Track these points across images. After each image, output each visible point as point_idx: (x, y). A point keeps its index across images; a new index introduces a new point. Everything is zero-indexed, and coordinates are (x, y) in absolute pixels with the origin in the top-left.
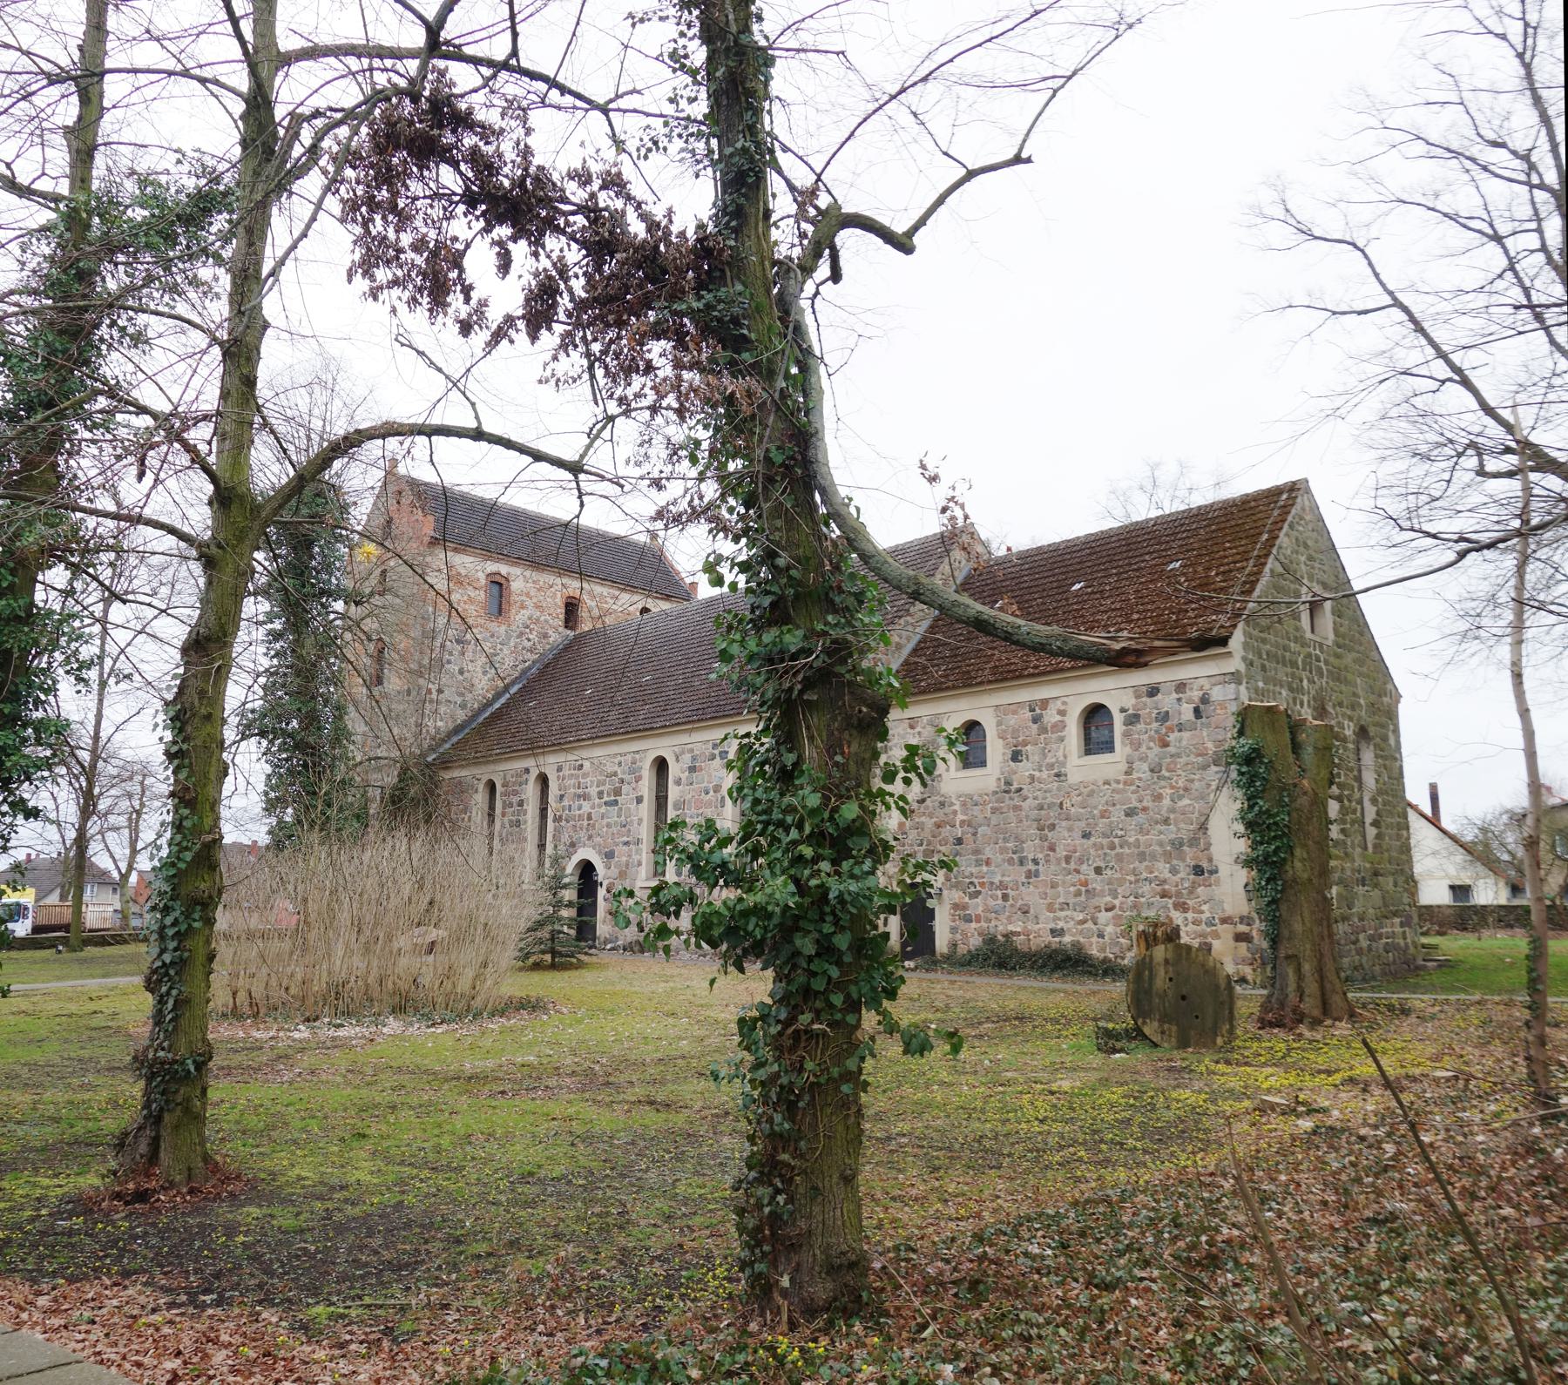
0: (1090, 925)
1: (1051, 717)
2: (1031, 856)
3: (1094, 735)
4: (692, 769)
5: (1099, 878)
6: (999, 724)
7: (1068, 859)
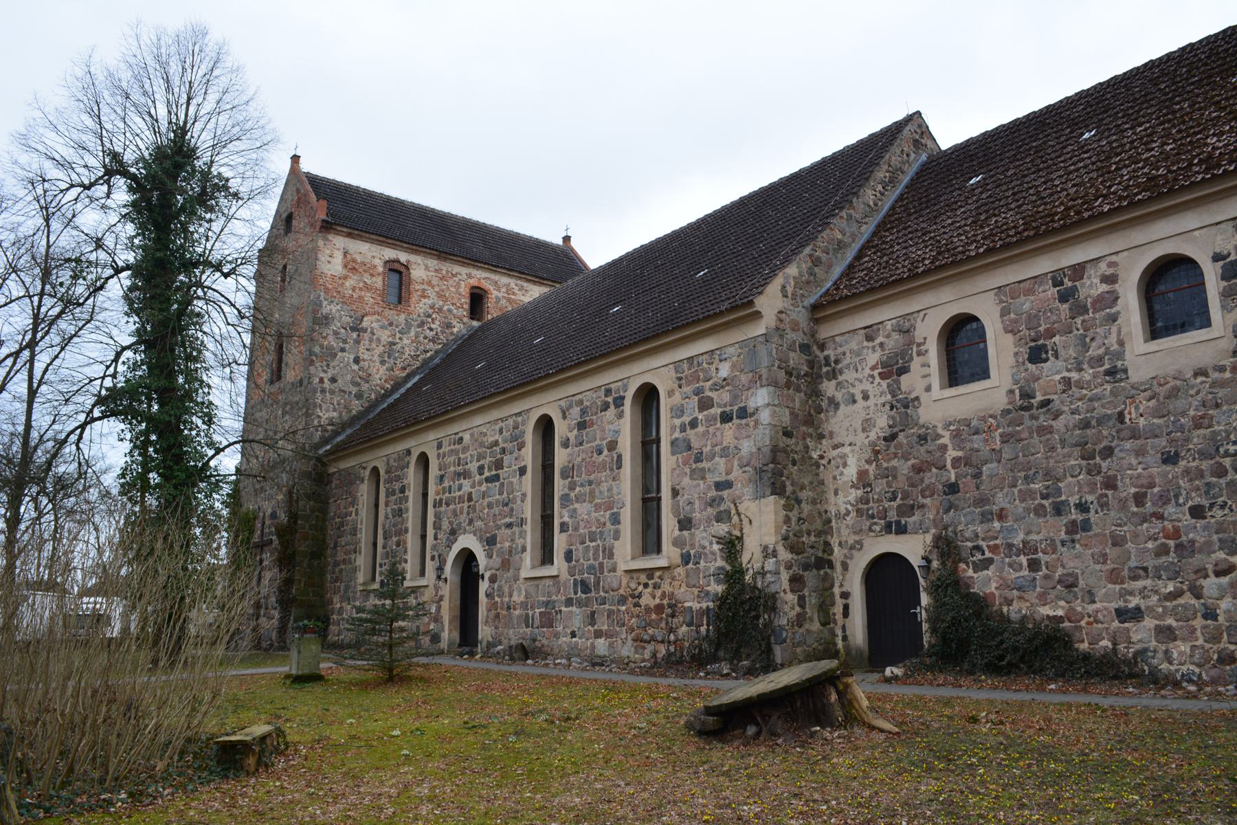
0: (1188, 599)
1: (1092, 287)
2: (1074, 500)
3: (1157, 307)
4: (582, 426)
5: (1200, 523)
6: (1004, 313)
7: (1139, 499)
